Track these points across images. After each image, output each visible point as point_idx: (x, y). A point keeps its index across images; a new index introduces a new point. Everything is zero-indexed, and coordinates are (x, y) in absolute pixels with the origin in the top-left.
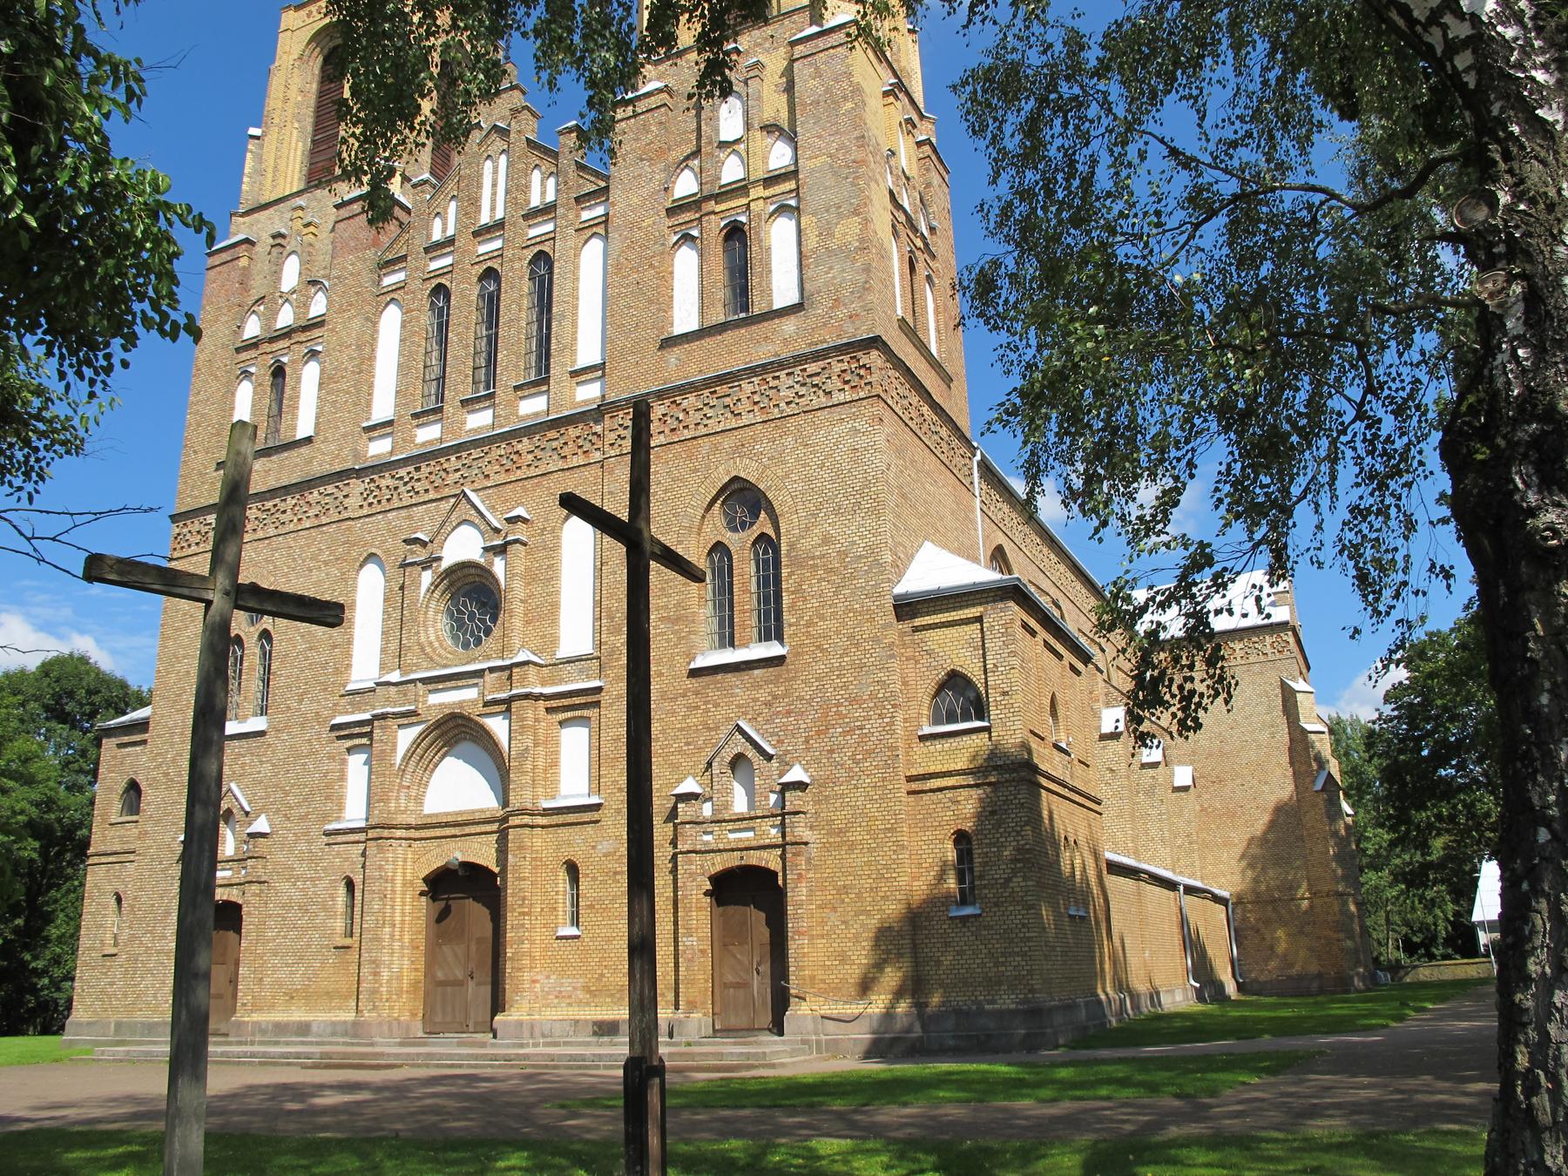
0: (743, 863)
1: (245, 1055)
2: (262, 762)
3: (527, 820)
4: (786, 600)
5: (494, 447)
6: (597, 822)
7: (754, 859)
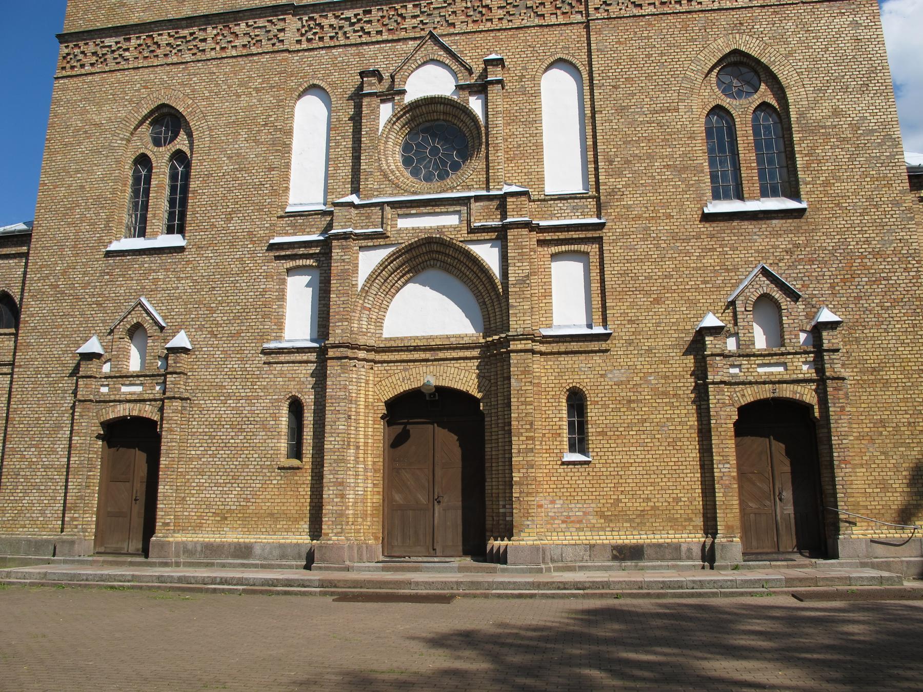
0: (776, 395)
1: (213, 581)
2: (179, 279)
3: (529, 345)
4: (800, 162)
6: (606, 351)
7: (787, 392)
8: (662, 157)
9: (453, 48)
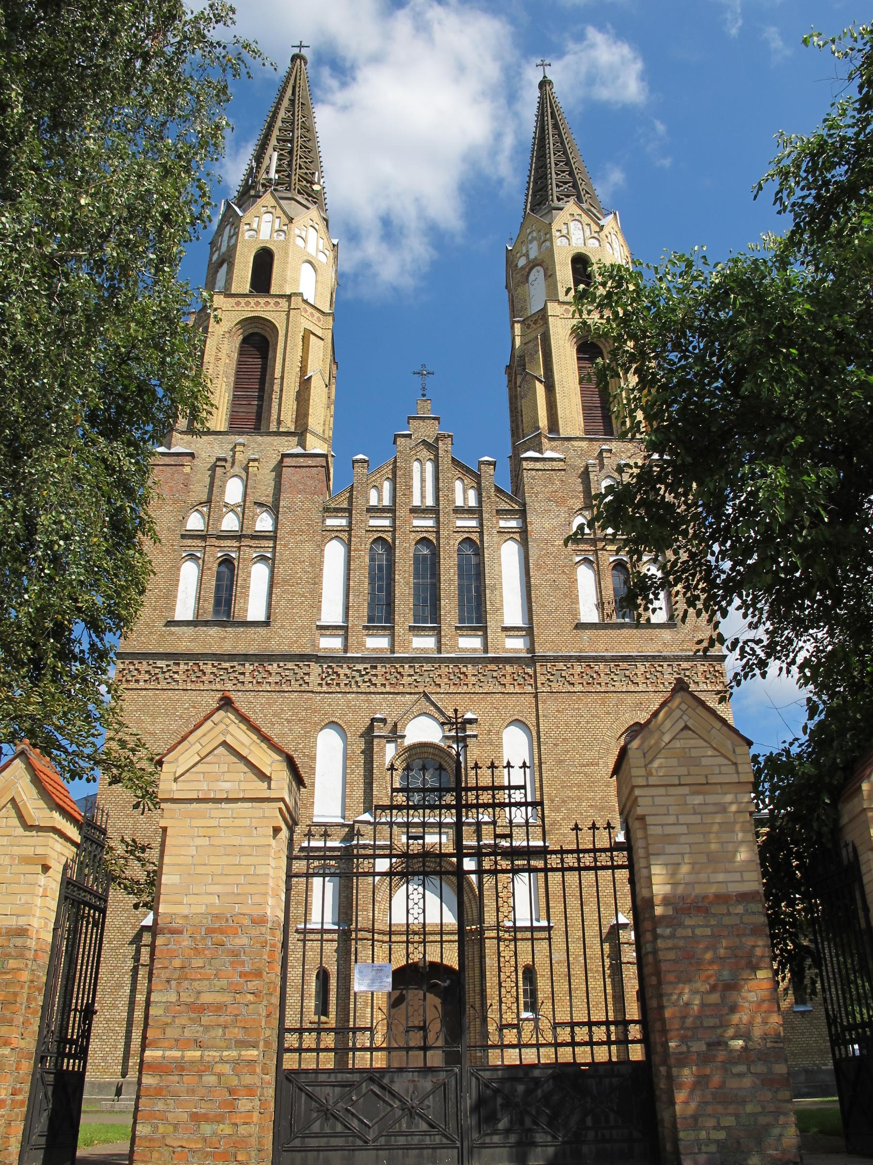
5: (443, 666)
8: (588, 799)
9: (439, 704)
